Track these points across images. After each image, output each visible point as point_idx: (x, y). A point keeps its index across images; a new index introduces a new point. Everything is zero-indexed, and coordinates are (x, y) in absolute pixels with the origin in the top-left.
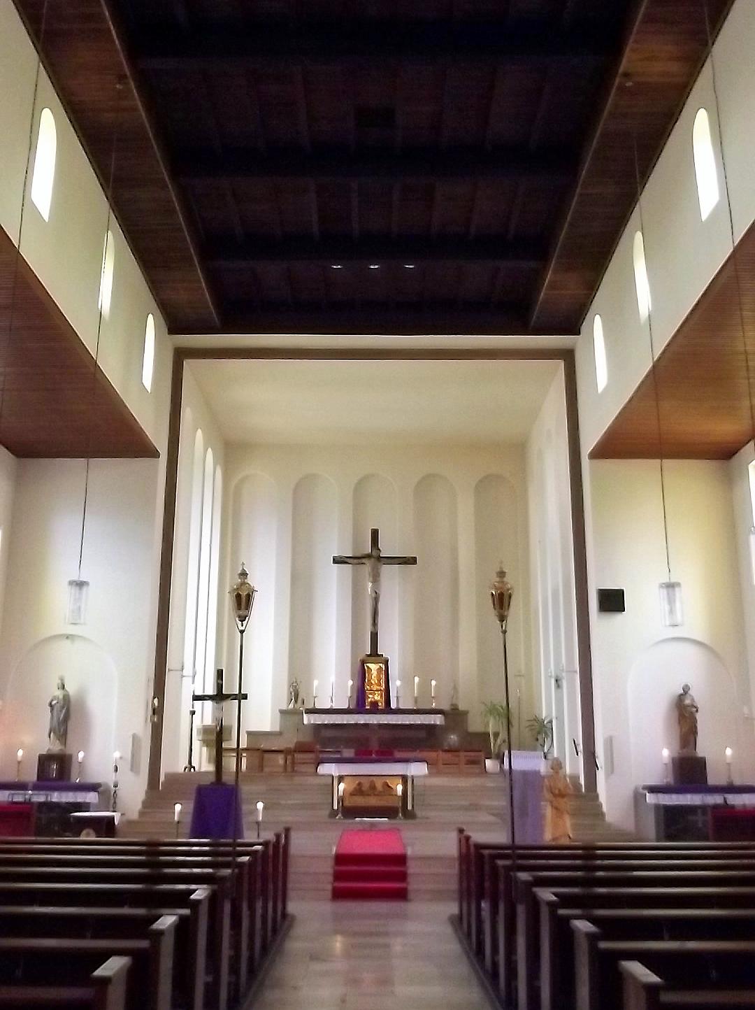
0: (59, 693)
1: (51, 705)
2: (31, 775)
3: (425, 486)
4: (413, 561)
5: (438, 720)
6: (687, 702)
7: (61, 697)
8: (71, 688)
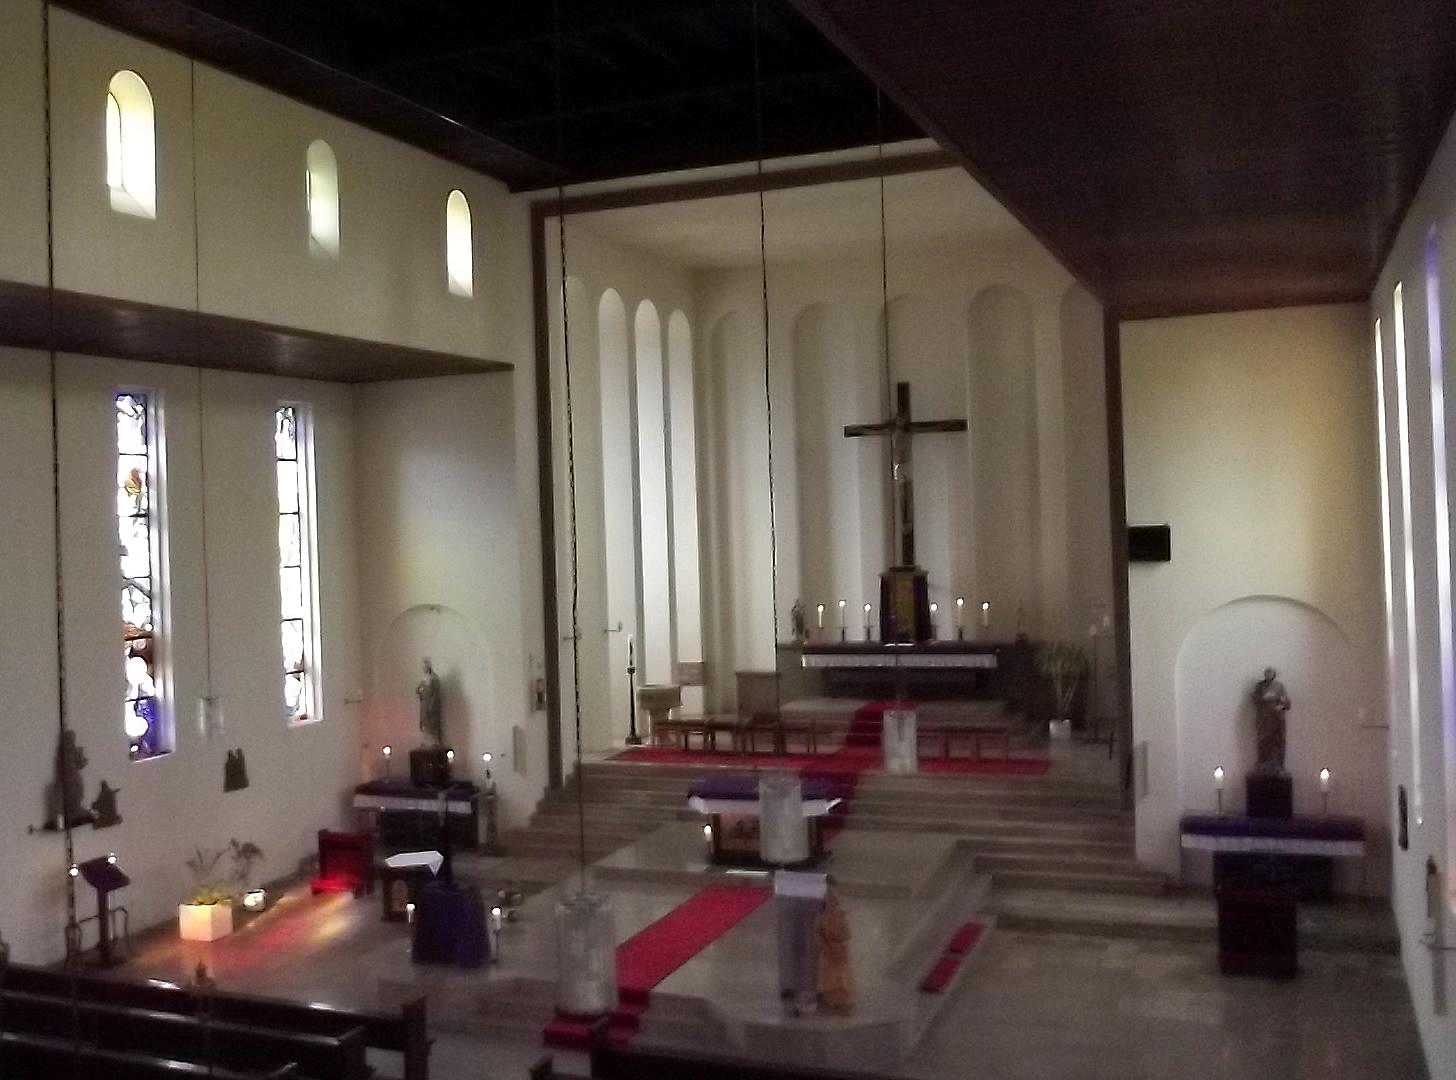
0: (426, 679)
1: (418, 692)
2: (404, 769)
3: (984, 306)
4: (959, 426)
5: (986, 661)
6: (1269, 694)
7: (428, 683)
8: (441, 670)
